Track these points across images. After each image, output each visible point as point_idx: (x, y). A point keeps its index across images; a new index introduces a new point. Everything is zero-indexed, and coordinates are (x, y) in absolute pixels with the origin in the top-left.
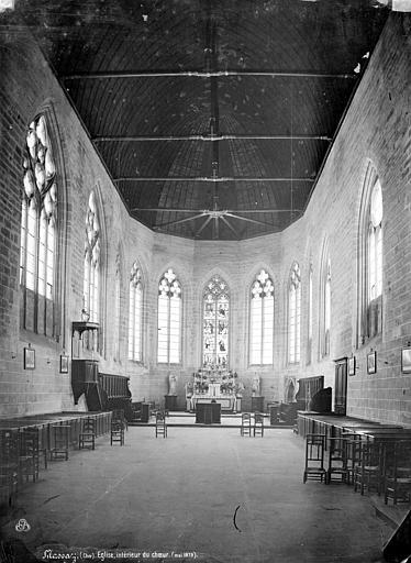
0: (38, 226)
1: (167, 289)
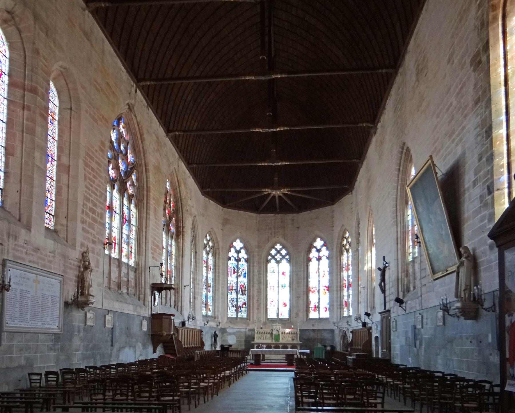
0: (122, 205)
1: (235, 255)
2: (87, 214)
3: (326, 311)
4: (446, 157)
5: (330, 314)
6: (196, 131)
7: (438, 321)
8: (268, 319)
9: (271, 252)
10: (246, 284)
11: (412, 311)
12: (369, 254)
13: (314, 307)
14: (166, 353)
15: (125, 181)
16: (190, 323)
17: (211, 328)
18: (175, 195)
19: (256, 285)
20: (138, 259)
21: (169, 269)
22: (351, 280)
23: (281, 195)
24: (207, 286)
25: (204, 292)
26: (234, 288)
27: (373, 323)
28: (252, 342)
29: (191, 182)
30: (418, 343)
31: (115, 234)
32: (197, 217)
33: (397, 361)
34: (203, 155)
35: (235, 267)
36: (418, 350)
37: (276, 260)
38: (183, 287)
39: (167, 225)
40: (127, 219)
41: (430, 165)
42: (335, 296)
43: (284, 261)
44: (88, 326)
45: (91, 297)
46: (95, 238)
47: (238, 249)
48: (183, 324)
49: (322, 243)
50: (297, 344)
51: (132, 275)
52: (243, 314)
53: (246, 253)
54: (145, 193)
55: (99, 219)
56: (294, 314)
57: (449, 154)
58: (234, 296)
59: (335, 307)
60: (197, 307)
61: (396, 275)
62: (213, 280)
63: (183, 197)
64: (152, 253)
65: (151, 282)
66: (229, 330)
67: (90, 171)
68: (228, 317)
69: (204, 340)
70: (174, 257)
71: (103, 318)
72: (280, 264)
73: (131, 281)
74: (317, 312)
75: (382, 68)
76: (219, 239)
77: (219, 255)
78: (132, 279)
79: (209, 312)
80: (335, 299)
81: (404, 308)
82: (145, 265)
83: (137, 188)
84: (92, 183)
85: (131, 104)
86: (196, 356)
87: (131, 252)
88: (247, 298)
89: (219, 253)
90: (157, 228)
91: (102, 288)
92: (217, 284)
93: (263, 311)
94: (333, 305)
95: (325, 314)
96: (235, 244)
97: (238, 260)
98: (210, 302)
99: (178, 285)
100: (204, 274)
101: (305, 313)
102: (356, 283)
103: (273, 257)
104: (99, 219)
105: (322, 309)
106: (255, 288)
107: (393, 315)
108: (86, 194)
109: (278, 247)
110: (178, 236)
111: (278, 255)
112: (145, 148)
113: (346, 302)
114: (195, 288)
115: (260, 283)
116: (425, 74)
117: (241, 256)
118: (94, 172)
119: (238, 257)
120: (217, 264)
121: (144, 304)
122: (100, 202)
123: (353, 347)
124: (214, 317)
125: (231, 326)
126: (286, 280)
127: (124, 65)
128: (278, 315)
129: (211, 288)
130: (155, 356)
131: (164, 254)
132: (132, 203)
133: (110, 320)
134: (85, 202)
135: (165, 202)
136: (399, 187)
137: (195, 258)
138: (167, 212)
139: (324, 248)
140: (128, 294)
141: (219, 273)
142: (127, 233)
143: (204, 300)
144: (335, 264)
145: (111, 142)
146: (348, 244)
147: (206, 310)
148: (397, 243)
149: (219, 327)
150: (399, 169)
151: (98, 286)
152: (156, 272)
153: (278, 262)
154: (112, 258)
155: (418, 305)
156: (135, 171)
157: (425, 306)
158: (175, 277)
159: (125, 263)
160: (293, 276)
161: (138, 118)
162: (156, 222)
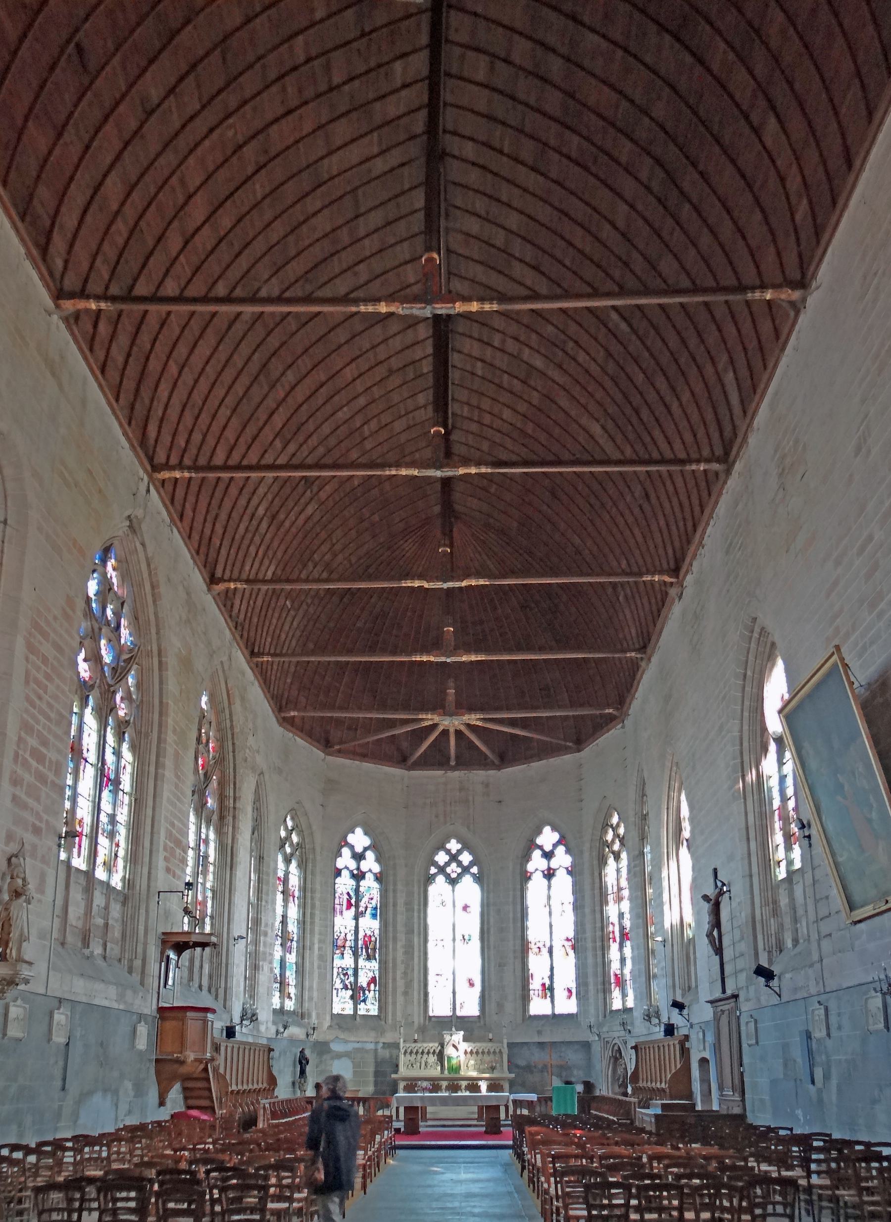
1: (352, 865)
2: (25, 764)
3: (569, 997)
4: (864, 649)
5: (579, 1005)
6: (271, 581)
7: (871, 1021)
8: (430, 1017)
9: (437, 858)
10: (377, 932)
11: (798, 996)
12: (673, 864)
13: (540, 988)
14: (189, 1107)
15: (112, 689)
16: (244, 1030)
17: (292, 1041)
18: (219, 723)
19: (402, 937)
20: (133, 872)
21: (200, 898)
22: (627, 923)
23: (462, 728)
24: (285, 937)
25: (278, 952)
26: (348, 944)
27: (691, 1026)
28: (393, 1076)
29: (256, 694)
30: (819, 1073)
31: (84, 811)
32: (267, 777)
33: (760, 1118)
34: (283, 636)
35: (352, 894)
36: (819, 1091)
37: (448, 876)
38: (232, 942)
39: (200, 793)
40: (112, 776)
41: (835, 665)
42: (590, 961)
43: (467, 879)
44: (11, 1039)
45: (25, 966)
46: (40, 819)
47: (359, 849)
48: (230, 1032)
49: (556, 837)
50: (503, 1079)
51: (116, 910)
52: (369, 1006)
53: (378, 860)
54: (156, 717)
55: (51, 776)
56: (492, 1007)
57: (872, 643)
58: (348, 961)
59: (591, 987)
60: (262, 990)
61: (749, 911)
62: (298, 923)
63: (237, 730)
64: (166, 859)
65: (161, 930)
66: (336, 1047)
67: (39, 663)
68: (332, 1015)
69: (275, 1073)
70: (211, 868)
71: (47, 1018)
72: (458, 887)
73: (113, 927)
74: (549, 999)
75: (698, 461)
76: (314, 828)
77: (314, 866)
78: (117, 921)
79: (287, 1002)
80: (590, 970)
81: (777, 989)
82: (149, 886)
83: (138, 706)
84: (41, 692)
85: (136, 517)
86: (262, 1111)
87: (116, 855)
88: (380, 968)
89: (314, 860)
90: (179, 799)
91: (48, 944)
92: (308, 936)
93: (419, 999)
94: (586, 984)
95: (567, 1006)
96: (351, 838)
97: (359, 876)
98: (291, 976)
99: (219, 936)
100: (279, 910)
101: (519, 1002)
102: (641, 931)
103: (442, 870)
104: (51, 776)
105: (560, 993)
106: (399, 944)
107: (745, 1007)
108: (25, 716)
109: (454, 846)
110: (222, 818)
111: (454, 865)
112: (160, 615)
113: (616, 975)
114: (256, 943)
115: (410, 931)
116: (799, 477)
117: (365, 866)
118: (46, 665)
119: (358, 868)
120: (309, 886)
121: (142, 983)
122: (56, 736)
123: (641, 1084)
124: (300, 1015)
125: (342, 1036)
126: (471, 924)
127: (125, 434)
128: (454, 1009)
129: (294, 944)
130: (164, 1114)
131: (190, 862)
132: (124, 740)
133: (63, 1022)
134: (23, 734)
135: (199, 740)
136: (746, 714)
137: (259, 871)
138: (200, 762)
139: (561, 849)
140: (105, 958)
141: (313, 907)
142: (110, 811)
143: (277, 971)
144: (587, 887)
145: (88, 600)
146: (617, 841)
147: (282, 997)
148: (748, 839)
149: (312, 1038)
150: (745, 675)
151: (40, 938)
152: (174, 904)
153: (453, 882)
154: (73, 870)
155: (812, 983)
156: (135, 667)
157: (831, 985)
158: (212, 917)
159: (101, 882)
160: (488, 914)
161: (150, 549)
162: (177, 786)
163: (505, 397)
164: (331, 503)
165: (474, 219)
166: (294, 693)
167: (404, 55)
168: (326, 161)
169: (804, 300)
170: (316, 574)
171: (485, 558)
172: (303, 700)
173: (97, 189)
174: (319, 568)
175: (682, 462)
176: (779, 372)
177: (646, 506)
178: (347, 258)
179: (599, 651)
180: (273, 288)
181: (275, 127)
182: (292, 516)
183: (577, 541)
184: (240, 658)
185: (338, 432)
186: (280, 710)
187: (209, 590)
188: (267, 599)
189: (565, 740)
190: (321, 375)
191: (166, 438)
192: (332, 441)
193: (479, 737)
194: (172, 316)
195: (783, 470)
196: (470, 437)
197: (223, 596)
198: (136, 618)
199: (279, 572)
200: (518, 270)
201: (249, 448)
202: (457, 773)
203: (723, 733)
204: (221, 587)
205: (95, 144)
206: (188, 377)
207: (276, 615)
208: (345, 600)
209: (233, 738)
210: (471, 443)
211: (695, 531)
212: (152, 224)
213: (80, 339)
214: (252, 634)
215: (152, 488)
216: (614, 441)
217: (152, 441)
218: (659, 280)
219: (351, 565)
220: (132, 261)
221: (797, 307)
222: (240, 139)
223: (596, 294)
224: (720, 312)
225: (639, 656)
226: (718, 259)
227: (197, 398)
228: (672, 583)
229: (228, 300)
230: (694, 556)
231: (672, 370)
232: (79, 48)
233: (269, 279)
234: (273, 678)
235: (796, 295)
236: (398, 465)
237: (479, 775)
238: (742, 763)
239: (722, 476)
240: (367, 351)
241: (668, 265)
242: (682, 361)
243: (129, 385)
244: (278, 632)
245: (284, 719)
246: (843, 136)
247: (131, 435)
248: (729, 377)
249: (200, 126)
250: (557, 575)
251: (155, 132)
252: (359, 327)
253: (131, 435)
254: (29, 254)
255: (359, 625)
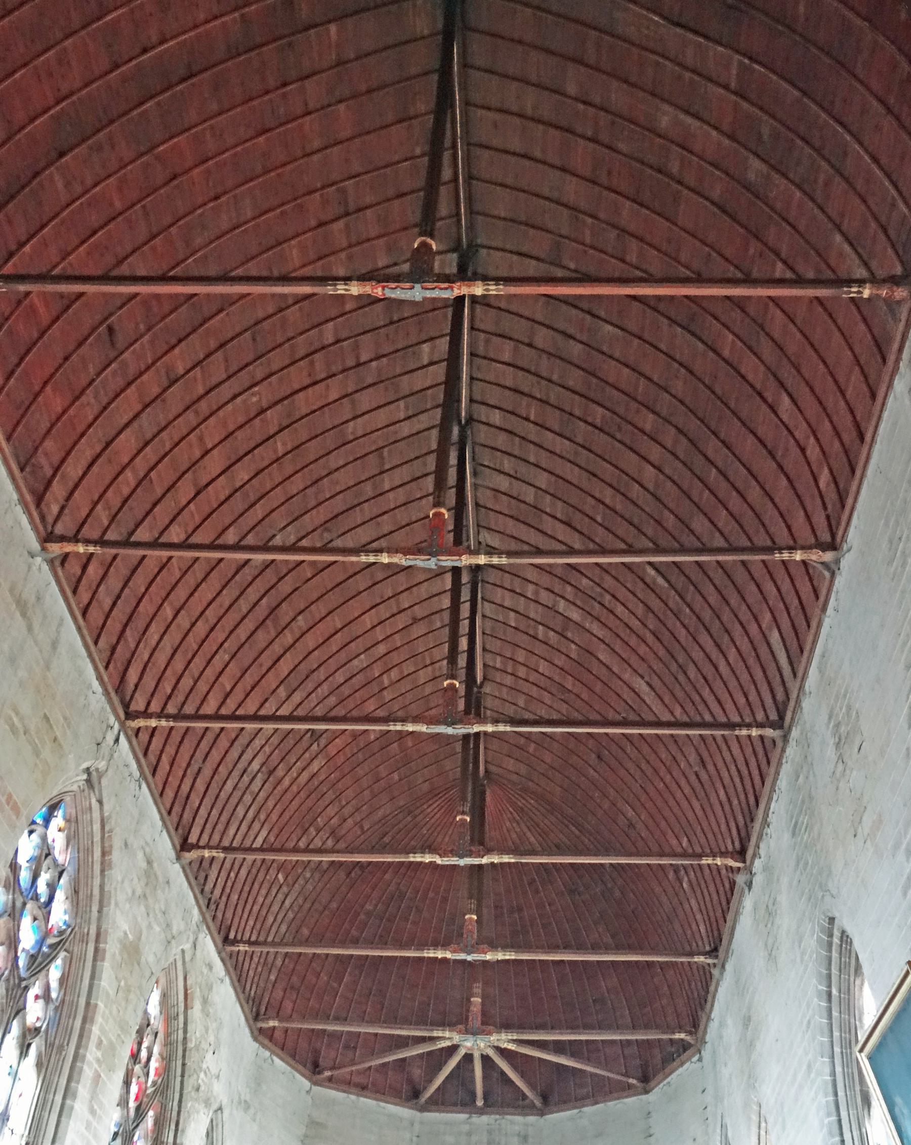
6: (261, 850)
18: (168, 1035)
23: (491, 1053)
34: (271, 919)
85: (97, 770)
127: (100, 678)
135: (135, 1057)
136: (837, 1050)
138: (134, 1089)
150: (829, 995)
156: (63, 954)
162: (88, 1126)
163: (540, 649)
164: (341, 759)
165: (502, 477)
166: (278, 994)
167: (432, 339)
168: (351, 424)
169: (837, 561)
170: (318, 843)
171: (525, 830)
172: (288, 1005)
173: (108, 444)
174: (324, 834)
175: (732, 726)
176: (824, 631)
177: (704, 776)
178: (368, 510)
179: (661, 955)
180: (290, 536)
181: (301, 394)
182: (294, 773)
183: (630, 813)
184: (208, 947)
185: (354, 680)
186: (256, 1018)
187: (178, 858)
188: (254, 871)
189: (626, 1075)
190: (337, 621)
191: (149, 682)
192: (346, 690)
193: (515, 1067)
194: (173, 560)
195: (840, 739)
196: (505, 690)
197: (195, 866)
198: (76, 892)
199: (272, 838)
200: (548, 524)
201: (247, 695)
202: (485, 1118)
203: (813, 1075)
204: (193, 855)
205: (113, 405)
206: (184, 621)
207: (263, 892)
208: (353, 874)
209: (184, 1056)
210: (505, 697)
211: (757, 805)
212: (162, 476)
213: (63, 580)
214: (229, 915)
215: (122, 738)
216: (662, 700)
217: (131, 686)
218: (692, 538)
219: (363, 832)
220: (138, 506)
221: (832, 570)
222: (265, 404)
223: (631, 550)
224: (759, 572)
225: (710, 961)
226: (749, 519)
227: (192, 642)
228: (739, 869)
229: (236, 547)
230: (760, 837)
231: (716, 627)
232: (110, 329)
233: (284, 527)
234: (251, 973)
235: (828, 556)
236: (403, 720)
237: (516, 1122)
238: (840, 1121)
239: (780, 744)
240: (389, 598)
241: (699, 524)
242: (725, 618)
243: (114, 626)
244: (264, 913)
245: (261, 1030)
246: (852, 412)
247: (106, 678)
248: (775, 637)
249: (226, 391)
250: (607, 853)
251: (176, 397)
252: (380, 576)
253: (106, 678)
254: (22, 501)
255: (368, 907)
